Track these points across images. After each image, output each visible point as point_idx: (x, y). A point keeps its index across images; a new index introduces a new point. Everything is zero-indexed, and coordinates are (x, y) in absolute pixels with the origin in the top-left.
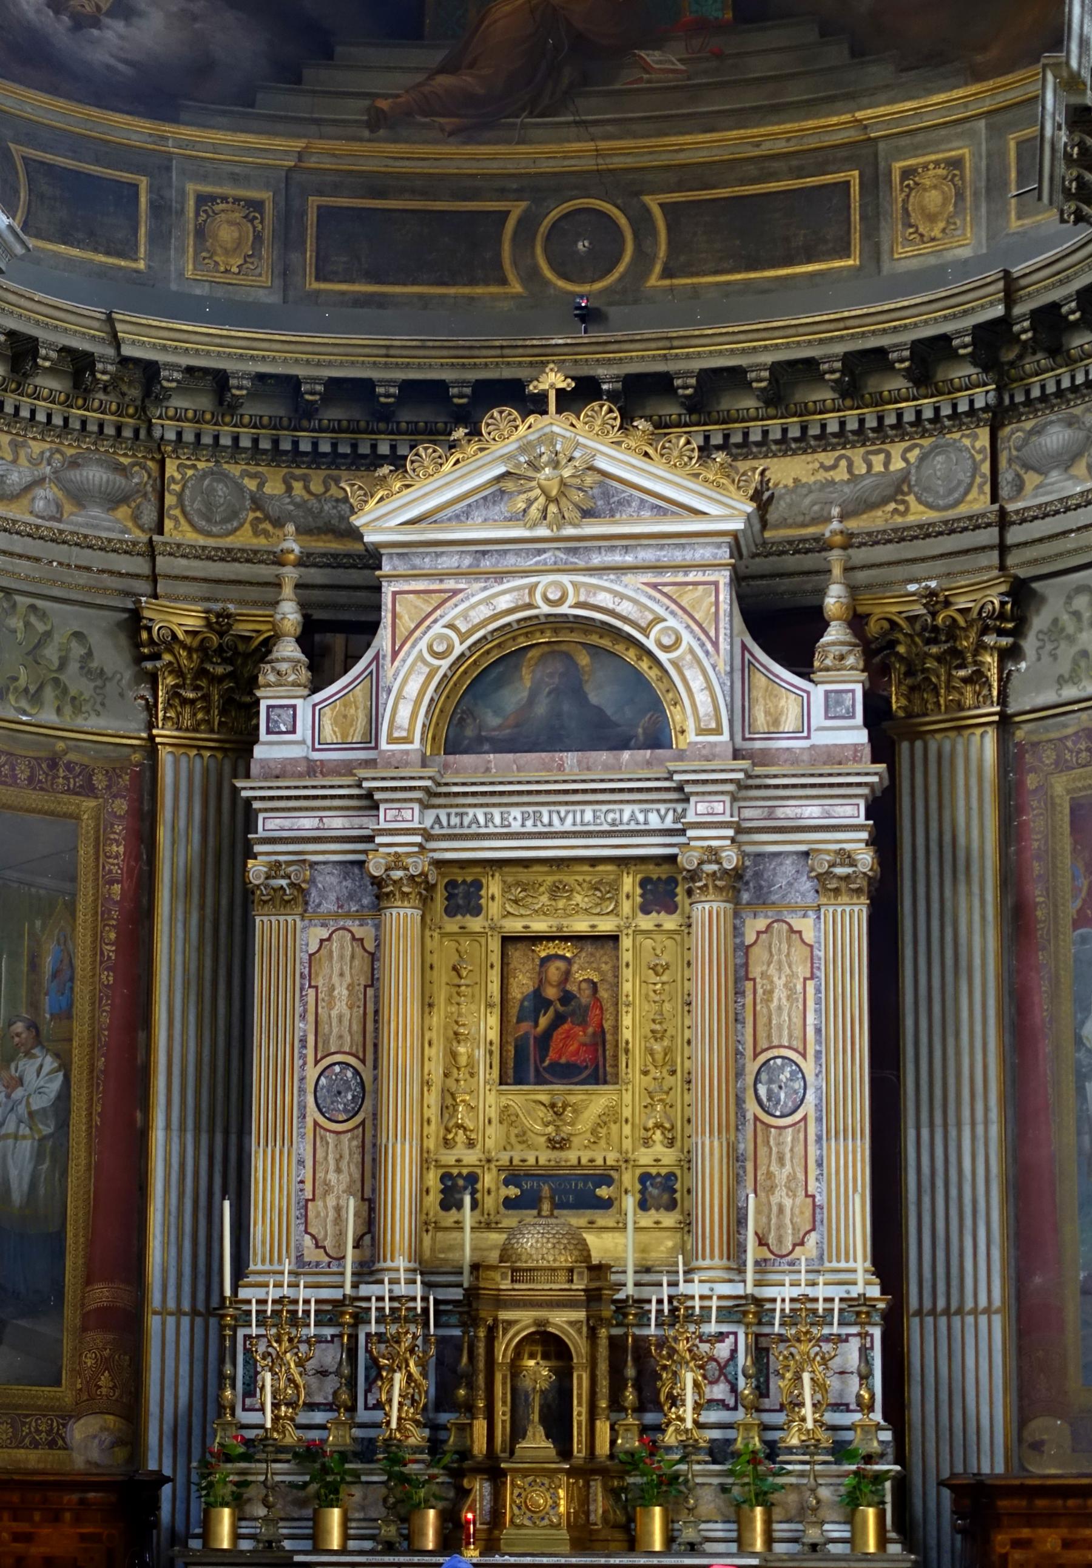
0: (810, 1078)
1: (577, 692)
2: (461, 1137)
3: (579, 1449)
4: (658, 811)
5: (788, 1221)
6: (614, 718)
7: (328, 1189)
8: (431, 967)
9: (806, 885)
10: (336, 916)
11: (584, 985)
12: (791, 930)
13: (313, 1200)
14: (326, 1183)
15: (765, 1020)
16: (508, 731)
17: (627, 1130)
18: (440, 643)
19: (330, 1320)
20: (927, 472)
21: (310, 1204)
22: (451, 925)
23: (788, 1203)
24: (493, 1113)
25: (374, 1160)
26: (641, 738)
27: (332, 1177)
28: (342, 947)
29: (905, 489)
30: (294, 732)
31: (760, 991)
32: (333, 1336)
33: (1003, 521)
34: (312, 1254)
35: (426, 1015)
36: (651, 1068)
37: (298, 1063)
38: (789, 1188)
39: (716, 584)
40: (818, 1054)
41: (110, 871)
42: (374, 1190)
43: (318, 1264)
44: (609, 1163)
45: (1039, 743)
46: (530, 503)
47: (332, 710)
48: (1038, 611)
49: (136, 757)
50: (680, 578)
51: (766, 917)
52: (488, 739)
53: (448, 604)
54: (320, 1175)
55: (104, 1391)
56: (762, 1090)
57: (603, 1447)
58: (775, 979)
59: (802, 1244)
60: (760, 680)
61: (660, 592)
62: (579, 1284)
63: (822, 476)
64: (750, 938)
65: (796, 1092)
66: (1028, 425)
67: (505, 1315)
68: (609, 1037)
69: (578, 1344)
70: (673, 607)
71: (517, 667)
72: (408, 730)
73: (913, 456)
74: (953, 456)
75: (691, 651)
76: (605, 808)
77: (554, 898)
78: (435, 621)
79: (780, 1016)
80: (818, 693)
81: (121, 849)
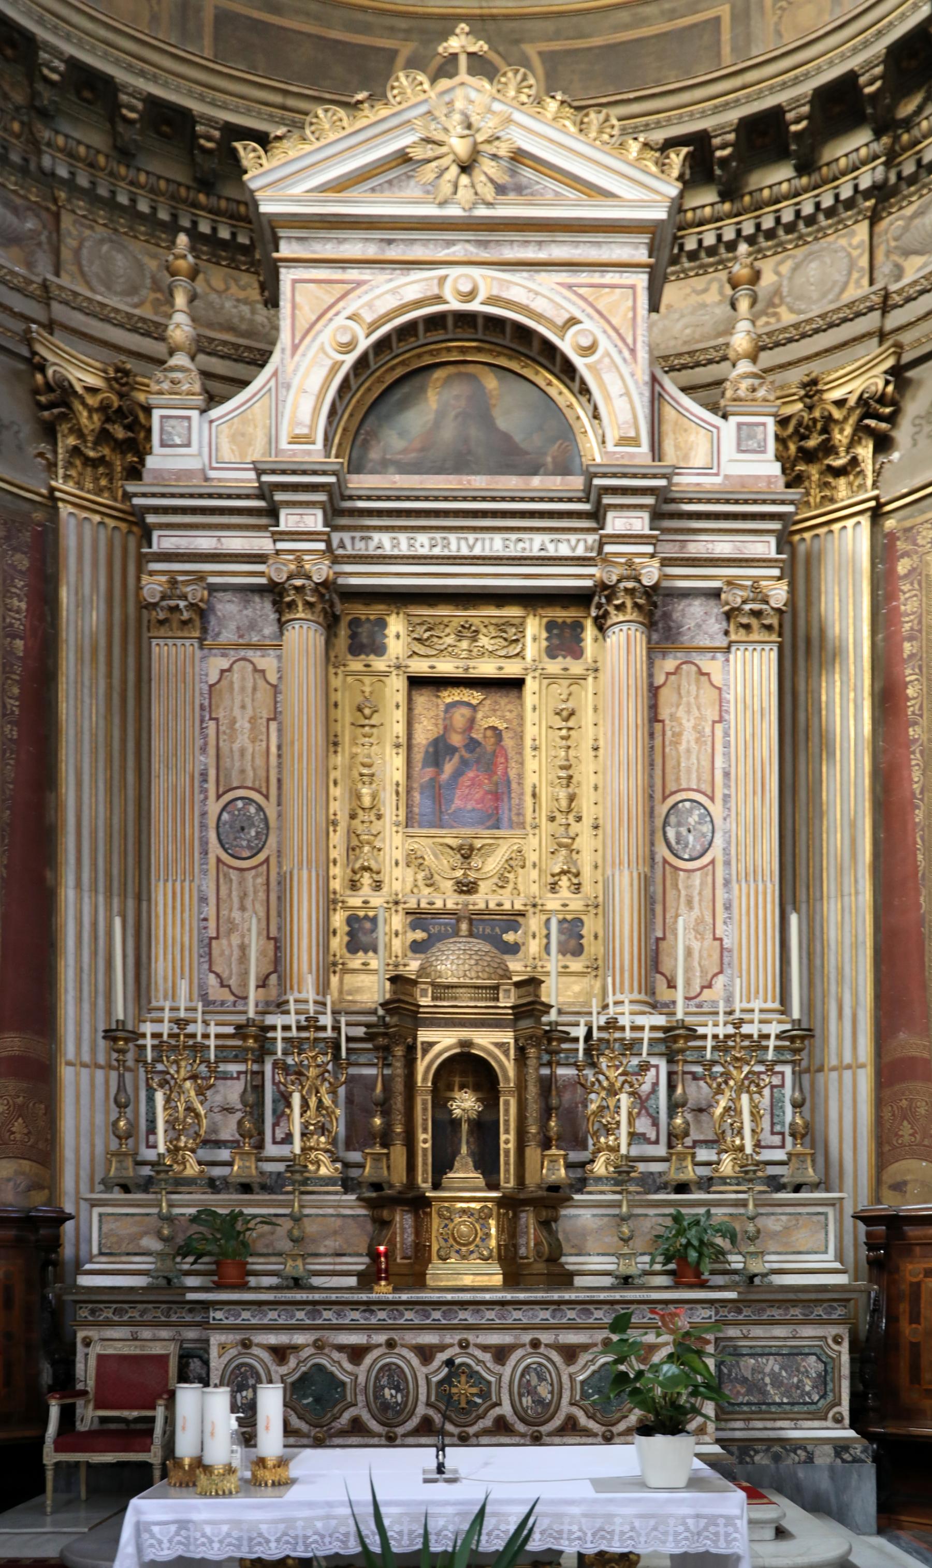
0: (718, 821)
1: (486, 418)
3: (508, 1180)
5: (696, 964)
6: (523, 445)
7: (233, 928)
8: (336, 705)
9: (715, 626)
10: (238, 646)
11: (489, 733)
12: (701, 673)
13: (217, 938)
14: (230, 921)
15: (674, 762)
16: (413, 455)
17: (534, 874)
19: (236, 1056)
20: (799, 280)
21: (214, 942)
22: (356, 665)
23: (696, 945)
24: (399, 855)
25: (279, 898)
26: (550, 467)
27: (236, 915)
28: (243, 679)
29: (777, 301)
30: (188, 445)
31: (669, 734)
32: (239, 1073)
33: (885, 306)
34: (216, 992)
35: (331, 754)
36: (557, 814)
37: (198, 797)
38: (697, 931)
39: (633, 287)
40: (726, 798)
41: (11, 625)
42: (279, 929)
43: (223, 1003)
45: (912, 528)
46: (443, 171)
47: (230, 427)
48: (913, 398)
49: (38, 516)
50: (596, 278)
51: (675, 658)
53: (351, 296)
54: (224, 913)
55: (18, 1136)
56: (671, 833)
57: (531, 1180)
58: (684, 721)
59: (710, 986)
60: (669, 413)
61: (576, 293)
62: (507, 1000)
63: (694, 299)
64: (659, 679)
65: (704, 835)
66: (908, 211)
67: (424, 1035)
68: (514, 786)
69: (507, 1067)
70: (590, 310)
71: (423, 389)
72: (311, 427)
73: (785, 269)
74: (828, 260)
75: (608, 354)
76: (514, 536)
77: (460, 637)
78: (337, 314)
79: (688, 759)
80: (728, 428)
81: (23, 606)
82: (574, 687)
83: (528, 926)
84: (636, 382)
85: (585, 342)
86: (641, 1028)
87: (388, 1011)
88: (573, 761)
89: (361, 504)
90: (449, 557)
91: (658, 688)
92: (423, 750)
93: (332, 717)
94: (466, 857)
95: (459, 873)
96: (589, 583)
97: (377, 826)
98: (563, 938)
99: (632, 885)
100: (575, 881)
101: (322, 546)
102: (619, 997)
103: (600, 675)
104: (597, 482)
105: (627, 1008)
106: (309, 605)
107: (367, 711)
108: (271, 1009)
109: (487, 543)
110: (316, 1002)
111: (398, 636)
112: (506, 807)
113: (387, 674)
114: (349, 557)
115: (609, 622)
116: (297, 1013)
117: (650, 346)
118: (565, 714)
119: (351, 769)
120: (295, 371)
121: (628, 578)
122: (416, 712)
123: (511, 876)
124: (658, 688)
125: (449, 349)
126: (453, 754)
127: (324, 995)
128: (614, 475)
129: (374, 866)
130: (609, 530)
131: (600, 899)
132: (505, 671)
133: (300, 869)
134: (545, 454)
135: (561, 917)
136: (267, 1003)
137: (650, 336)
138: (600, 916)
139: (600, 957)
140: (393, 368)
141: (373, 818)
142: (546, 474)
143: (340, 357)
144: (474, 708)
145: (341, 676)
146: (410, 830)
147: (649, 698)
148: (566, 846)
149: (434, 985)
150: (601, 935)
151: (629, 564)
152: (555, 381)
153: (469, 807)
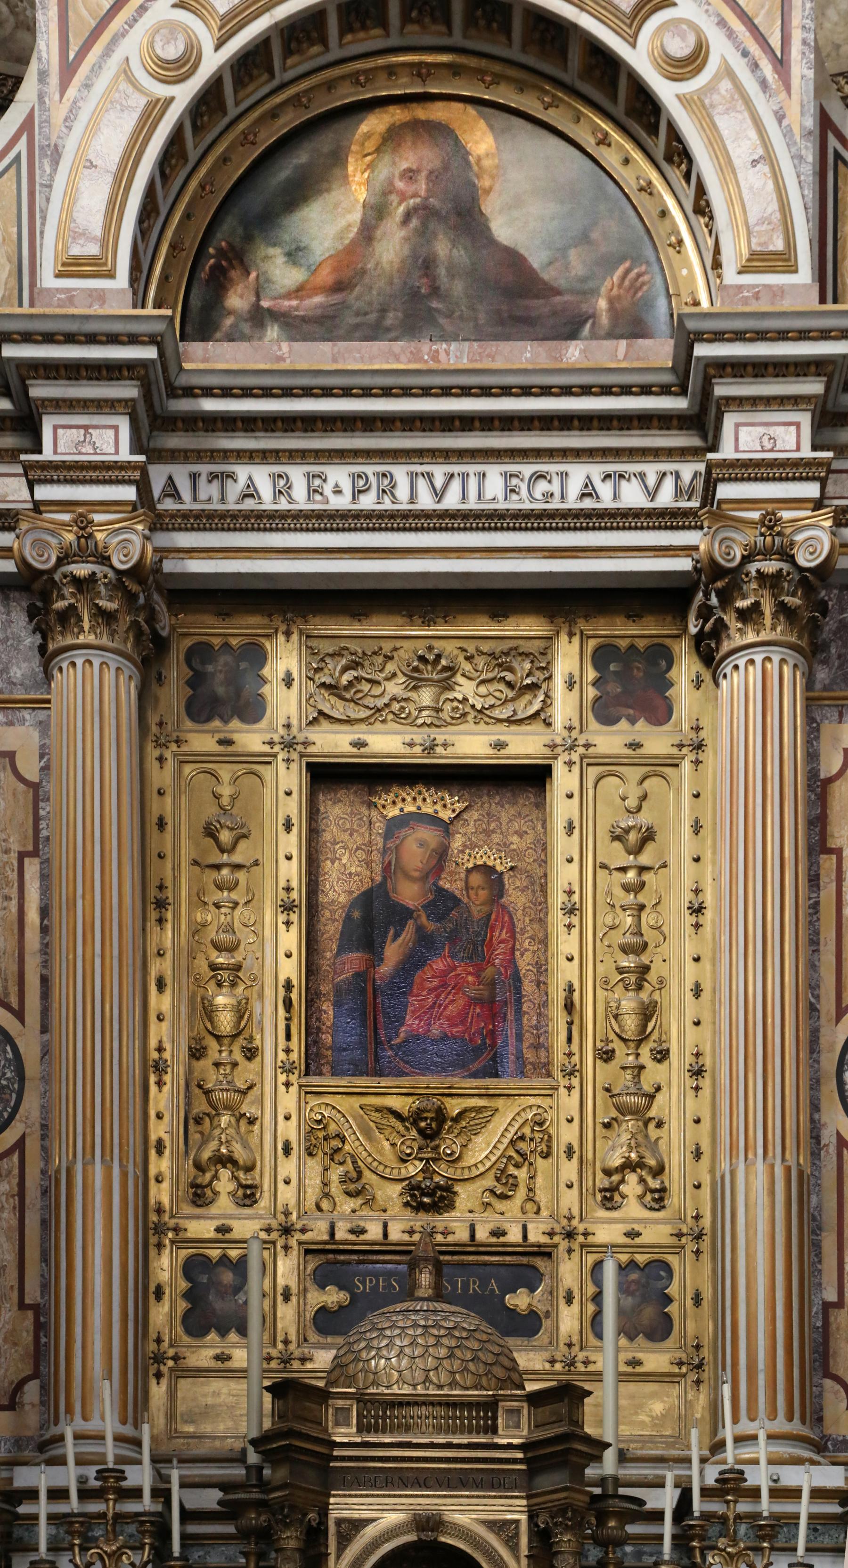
2: (225, 1183)
4: (642, 476)
6: (545, 276)
8: (161, 824)
11: (476, 879)
16: (318, 299)
17: (569, 1170)
18: (171, 37)
24: (290, 1131)
25: (44, 1223)
26: (604, 320)
35: (152, 924)
36: (617, 1045)
42: (44, 1287)
44: (532, 1238)
52: (275, 315)
68: (528, 987)
71: (338, 158)
72: (104, 243)
75: (728, 72)
76: (527, 470)
77: (416, 682)
82: (651, 784)
83: (556, 1277)
84: (788, 133)
85: (680, 48)
86: (794, 1494)
87: (268, 1456)
88: (649, 935)
89: (210, 405)
90: (392, 515)
91: (830, 780)
92: (340, 915)
93: (153, 848)
94: (430, 1135)
95: (414, 1169)
96: (684, 564)
97: (246, 1072)
98: (629, 1301)
99: (772, 1192)
100: (654, 1184)
101: (129, 493)
102: (746, 1427)
103: (707, 756)
104: (701, 350)
105: (762, 1450)
106: (106, 617)
107: (225, 837)
108: (27, 1454)
109: (473, 483)
110: (119, 1439)
111: (288, 681)
112: (511, 1032)
113: (266, 760)
114: (186, 515)
115: (726, 646)
116: (79, 1463)
117: (817, 50)
118: (633, 837)
119: (192, 956)
120: (69, 121)
121: (766, 553)
122: (327, 836)
123: (522, 1174)
124: (830, 780)
125: (391, 71)
126: (402, 924)
127: (136, 1425)
128: (739, 336)
129: (240, 1153)
130: (727, 452)
131: (706, 1222)
132: (511, 750)
133: (88, 1163)
134: (594, 292)
135: (624, 1258)
136: (18, 1443)
137: (819, 26)
138: (706, 1258)
139: (706, 1342)
140: (273, 114)
141: (238, 1056)
142: (594, 336)
143: (162, 91)
144: (446, 828)
145: (170, 764)
146: (314, 1080)
147: (809, 803)
148: (637, 1112)
149: (361, 1399)
150: (707, 1294)
151: (770, 523)
152: (616, 136)
153: (435, 1031)
